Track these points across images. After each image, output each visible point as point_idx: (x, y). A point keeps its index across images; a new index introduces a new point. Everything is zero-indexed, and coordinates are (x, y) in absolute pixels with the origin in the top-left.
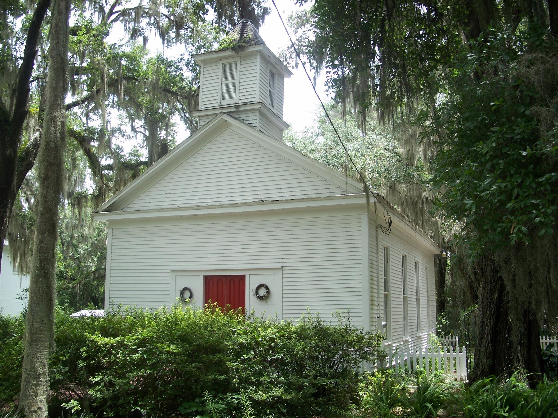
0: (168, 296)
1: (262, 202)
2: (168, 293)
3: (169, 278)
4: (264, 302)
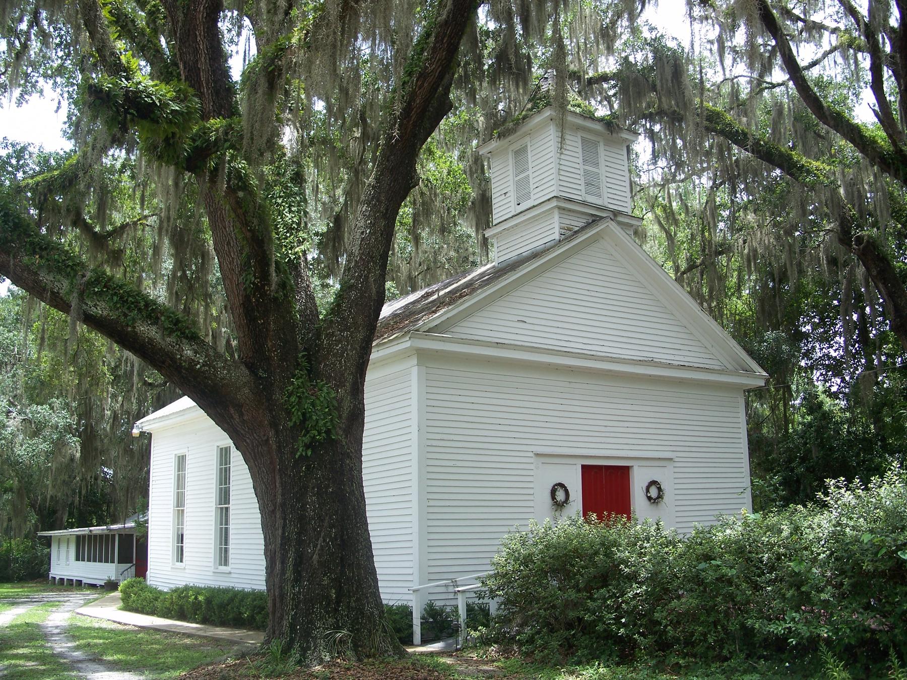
0: (531, 498)
1: (651, 363)
2: (531, 492)
3: (532, 467)
4: (654, 507)
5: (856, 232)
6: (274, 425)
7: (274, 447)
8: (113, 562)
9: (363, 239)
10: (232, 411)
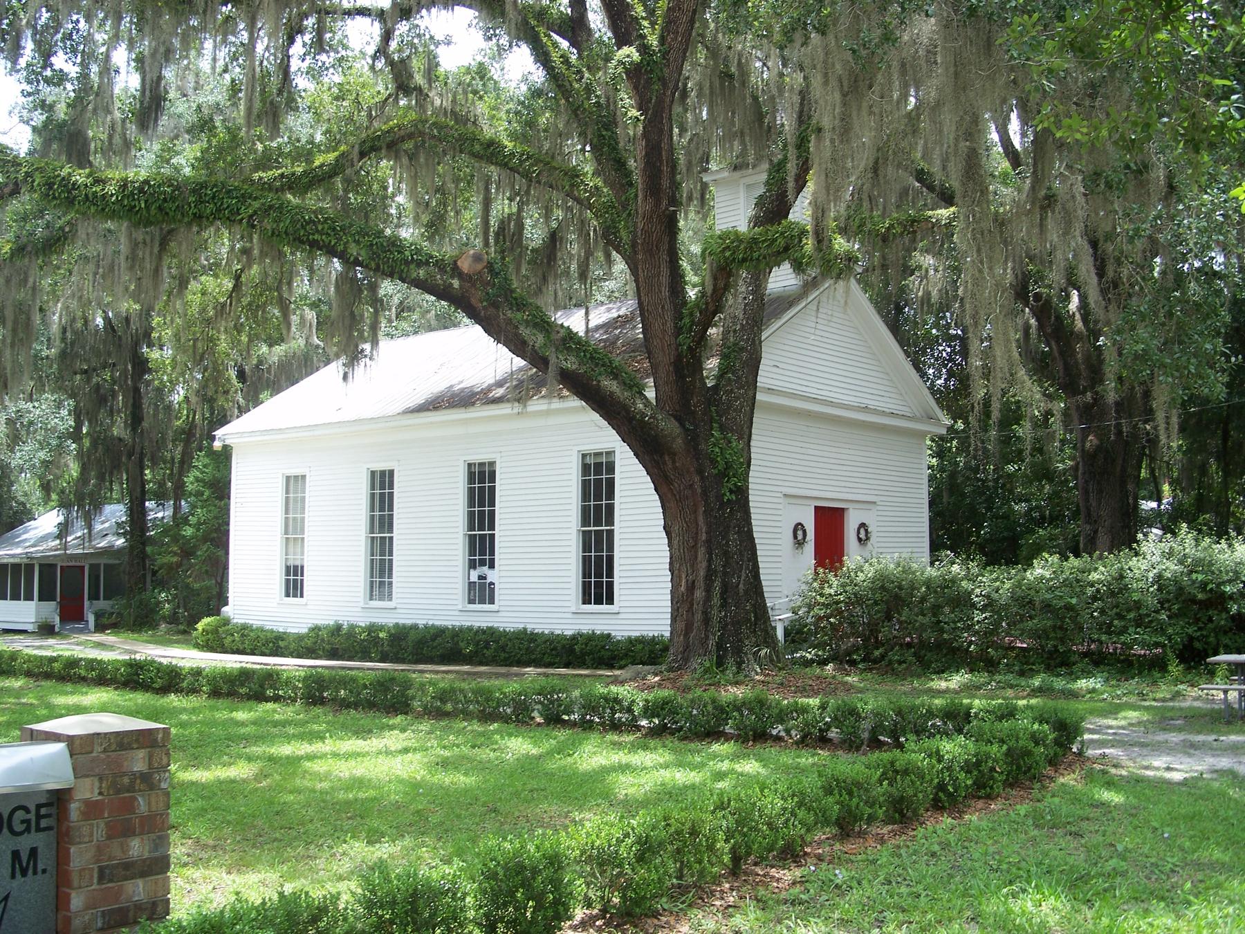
1: (866, 409)
5: (1034, 289)
6: (700, 472)
7: (699, 491)
8: (29, 598)
9: (746, 305)
10: (667, 458)
